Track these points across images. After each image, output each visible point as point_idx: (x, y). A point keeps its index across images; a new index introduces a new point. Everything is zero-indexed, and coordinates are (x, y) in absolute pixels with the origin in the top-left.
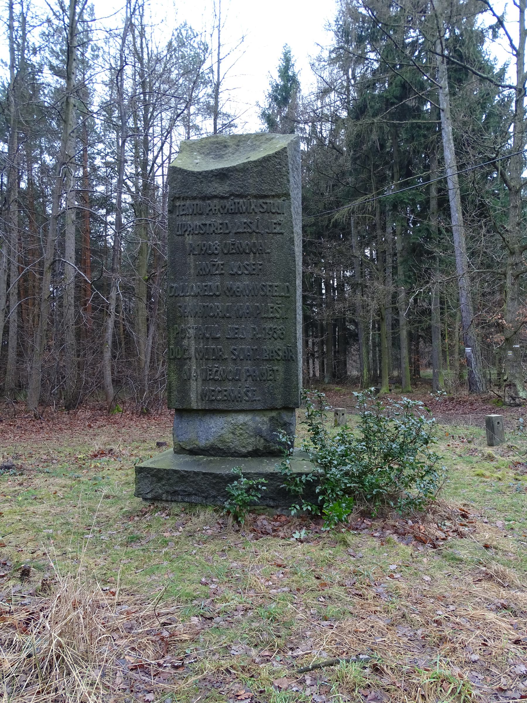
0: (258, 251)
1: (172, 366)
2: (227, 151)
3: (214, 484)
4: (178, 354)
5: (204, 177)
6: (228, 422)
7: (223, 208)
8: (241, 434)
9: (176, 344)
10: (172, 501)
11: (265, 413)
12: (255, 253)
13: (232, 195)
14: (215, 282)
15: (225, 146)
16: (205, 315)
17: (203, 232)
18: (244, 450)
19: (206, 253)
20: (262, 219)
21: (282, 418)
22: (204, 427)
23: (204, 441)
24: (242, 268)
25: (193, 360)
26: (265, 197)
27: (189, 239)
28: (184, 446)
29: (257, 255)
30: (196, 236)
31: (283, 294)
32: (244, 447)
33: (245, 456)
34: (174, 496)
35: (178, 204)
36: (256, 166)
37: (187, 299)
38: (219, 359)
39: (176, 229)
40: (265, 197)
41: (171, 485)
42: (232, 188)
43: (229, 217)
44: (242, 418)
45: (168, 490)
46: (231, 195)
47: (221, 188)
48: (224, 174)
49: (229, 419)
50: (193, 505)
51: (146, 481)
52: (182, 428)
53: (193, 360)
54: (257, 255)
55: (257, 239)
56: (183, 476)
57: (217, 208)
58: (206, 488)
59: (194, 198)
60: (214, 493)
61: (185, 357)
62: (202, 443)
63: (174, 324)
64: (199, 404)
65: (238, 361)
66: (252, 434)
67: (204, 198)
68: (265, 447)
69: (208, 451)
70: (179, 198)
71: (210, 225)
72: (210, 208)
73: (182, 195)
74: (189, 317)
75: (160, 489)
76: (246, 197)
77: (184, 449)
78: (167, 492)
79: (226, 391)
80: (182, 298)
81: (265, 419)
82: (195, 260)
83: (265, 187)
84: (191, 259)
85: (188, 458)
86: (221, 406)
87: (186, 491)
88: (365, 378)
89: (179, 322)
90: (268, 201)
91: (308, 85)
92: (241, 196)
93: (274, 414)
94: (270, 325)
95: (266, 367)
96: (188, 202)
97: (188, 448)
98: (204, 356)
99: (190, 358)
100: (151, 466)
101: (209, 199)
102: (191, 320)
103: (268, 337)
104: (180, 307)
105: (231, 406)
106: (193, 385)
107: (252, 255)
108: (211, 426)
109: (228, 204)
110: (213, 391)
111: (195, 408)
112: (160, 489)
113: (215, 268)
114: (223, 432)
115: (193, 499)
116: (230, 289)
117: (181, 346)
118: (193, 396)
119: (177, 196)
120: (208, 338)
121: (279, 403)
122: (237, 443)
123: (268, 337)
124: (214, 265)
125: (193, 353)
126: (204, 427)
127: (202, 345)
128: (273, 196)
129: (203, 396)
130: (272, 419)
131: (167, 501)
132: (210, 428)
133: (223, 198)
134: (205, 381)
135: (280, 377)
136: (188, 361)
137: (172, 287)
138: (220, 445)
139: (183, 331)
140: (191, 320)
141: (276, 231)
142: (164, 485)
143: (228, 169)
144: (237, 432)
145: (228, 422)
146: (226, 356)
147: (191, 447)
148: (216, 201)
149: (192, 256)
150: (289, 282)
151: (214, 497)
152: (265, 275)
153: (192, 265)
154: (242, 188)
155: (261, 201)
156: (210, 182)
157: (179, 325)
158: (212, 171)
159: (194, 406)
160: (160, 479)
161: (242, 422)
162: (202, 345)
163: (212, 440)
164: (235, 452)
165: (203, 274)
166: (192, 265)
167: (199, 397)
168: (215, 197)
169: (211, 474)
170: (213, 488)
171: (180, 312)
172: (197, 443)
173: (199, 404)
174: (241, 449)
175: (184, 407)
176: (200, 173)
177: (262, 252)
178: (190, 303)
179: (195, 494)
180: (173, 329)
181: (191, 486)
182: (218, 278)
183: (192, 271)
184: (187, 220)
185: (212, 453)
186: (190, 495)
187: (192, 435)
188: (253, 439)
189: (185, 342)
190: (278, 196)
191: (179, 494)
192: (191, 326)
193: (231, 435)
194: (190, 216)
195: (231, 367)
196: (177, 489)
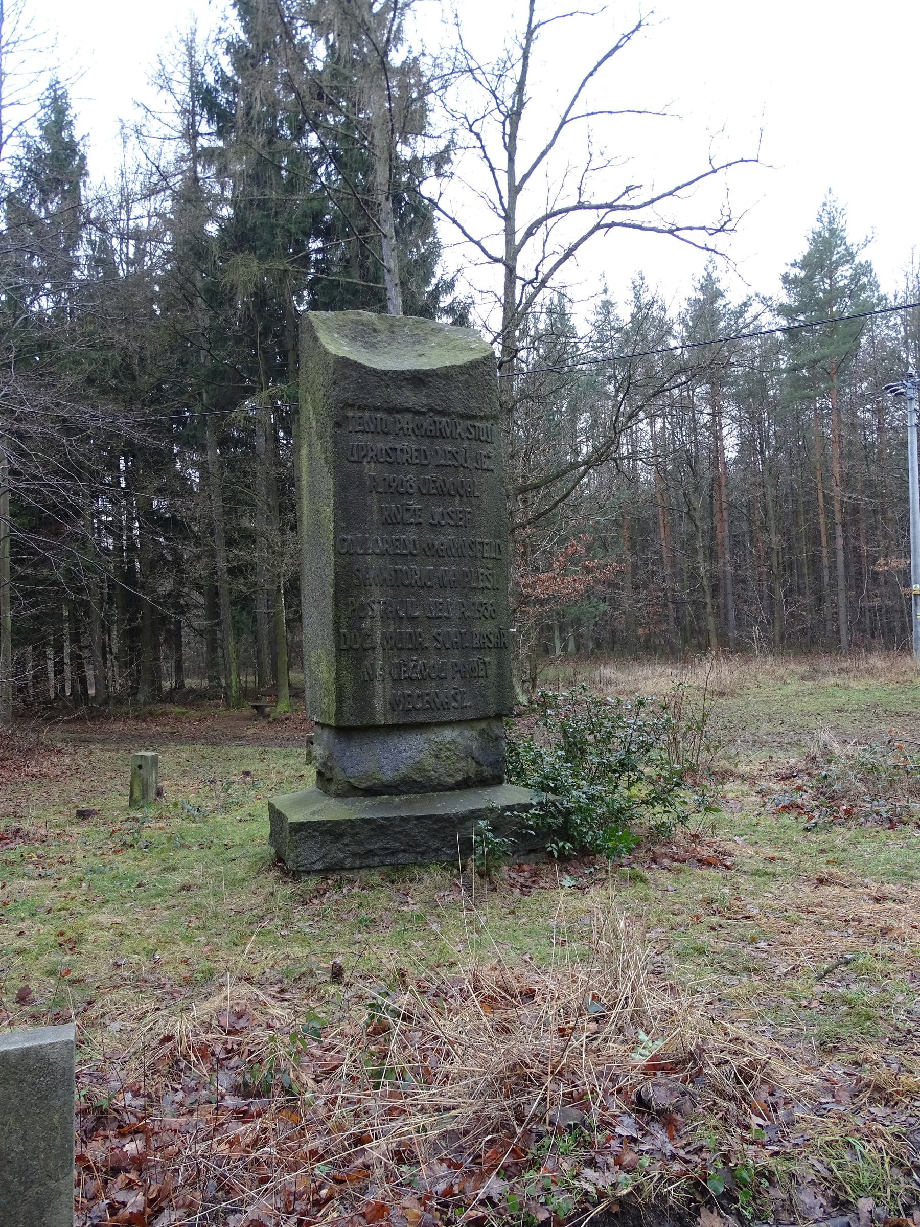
0: (467, 493)
1: (344, 661)
2: (379, 339)
3: (436, 830)
4: (356, 642)
5: (391, 379)
6: (428, 741)
7: (420, 427)
8: (448, 757)
9: (351, 627)
10: (361, 868)
11: (475, 724)
12: (461, 496)
13: (432, 410)
14: (410, 535)
15: (375, 331)
16: (398, 583)
17: (391, 458)
18: (451, 780)
19: (396, 492)
20: (470, 448)
21: (493, 731)
22: (390, 751)
23: (390, 773)
24: (446, 516)
25: (379, 650)
26: (473, 417)
27: (370, 469)
28: (356, 784)
29: (465, 499)
30: (380, 466)
31: (493, 555)
32: (451, 775)
33: (451, 788)
34: (365, 859)
35: (350, 414)
36: (462, 374)
37: (369, 558)
38: (419, 649)
39: (349, 452)
40: (473, 417)
41: (361, 843)
42: (430, 401)
43: (428, 441)
44: (449, 734)
45: (356, 850)
46: (429, 410)
47: (411, 398)
48: (420, 379)
49: (432, 736)
50: (398, 868)
51: (311, 843)
52: (351, 756)
53: (379, 650)
54: (465, 499)
55: (464, 477)
56: (381, 826)
57: (410, 426)
58: (423, 838)
59: (376, 409)
60: (437, 844)
61: (366, 646)
62: (388, 775)
63: (347, 597)
64: (389, 717)
65: (443, 651)
66: (462, 755)
67: (393, 410)
68: (478, 773)
69: (396, 787)
70: (352, 406)
71: (401, 450)
72: (400, 426)
73: (359, 402)
74: (373, 587)
75: (307, 857)
76: (449, 415)
77: (356, 788)
78: (354, 855)
79: (427, 695)
80: (360, 557)
81: (474, 733)
82: (379, 501)
83: (473, 403)
84: (373, 500)
85: (367, 801)
86: (422, 718)
87: (387, 849)
88: (234, 688)
89: (355, 592)
90: (477, 424)
91: (107, 169)
92: (442, 413)
93: (483, 725)
94: (480, 598)
95: (476, 657)
96: (367, 414)
97: (363, 786)
98: (394, 644)
99: (374, 649)
100: (317, 818)
101: (398, 412)
102: (376, 591)
103: (477, 615)
104: (358, 570)
105: (436, 716)
106: (379, 687)
107: (458, 498)
108: (402, 749)
109: (426, 422)
110: (409, 696)
111: (382, 723)
112: (307, 857)
113: (409, 515)
114: (422, 755)
115: (401, 858)
116: (431, 547)
117: (360, 630)
118: (378, 705)
119: (350, 402)
120: (401, 618)
121: (492, 709)
122: (441, 770)
123: (477, 615)
124: (408, 510)
125: (379, 640)
126: (390, 751)
127: (392, 627)
128: (482, 418)
129: (393, 705)
130: (482, 732)
131: (352, 869)
132: (401, 752)
133: (418, 413)
134: (397, 681)
135: (493, 671)
136: (370, 652)
137: (344, 540)
138: (417, 777)
139: (363, 607)
140: (376, 591)
141: (485, 466)
142: (346, 845)
143: (425, 373)
144: (443, 755)
145: (428, 741)
146: (427, 644)
147: (369, 783)
148: (408, 416)
149: (374, 494)
150: (500, 538)
151: (437, 850)
152: (474, 527)
153: (375, 507)
154: (444, 401)
155: (469, 423)
156: (400, 387)
157: (357, 597)
158: (402, 372)
159: (380, 720)
160: (341, 836)
161: (449, 739)
162: (392, 627)
163: (403, 769)
164: (439, 784)
165: (391, 522)
166: (375, 507)
167: (388, 706)
168: (407, 410)
169: (430, 817)
170: (435, 836)
171: (358, 578)
172: (379, 776)
173: (389, 717)
174: (447, 779)
175: (365, 723)
176: (386, 373)
177: (470, 495)
178: (373, 565)
179: (404, 851)
180: (347, 605)
181: (396, 840)
182: (414, 529)
183: (375, 517)
184: (367, 440)
185: (404, 789)
186: (394, 852)
187: (370, 766)
188: (463, 763)
189: (366, 624)
190: (485, 418)
191: (376, 855)
192: (377, 599)
193: (434, 760)
194: (370, 435)
195: (433, 659)
196: (372, 847)
